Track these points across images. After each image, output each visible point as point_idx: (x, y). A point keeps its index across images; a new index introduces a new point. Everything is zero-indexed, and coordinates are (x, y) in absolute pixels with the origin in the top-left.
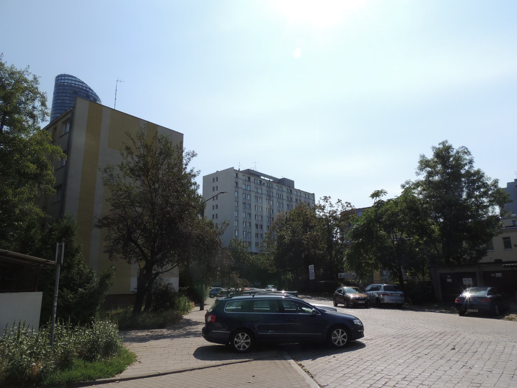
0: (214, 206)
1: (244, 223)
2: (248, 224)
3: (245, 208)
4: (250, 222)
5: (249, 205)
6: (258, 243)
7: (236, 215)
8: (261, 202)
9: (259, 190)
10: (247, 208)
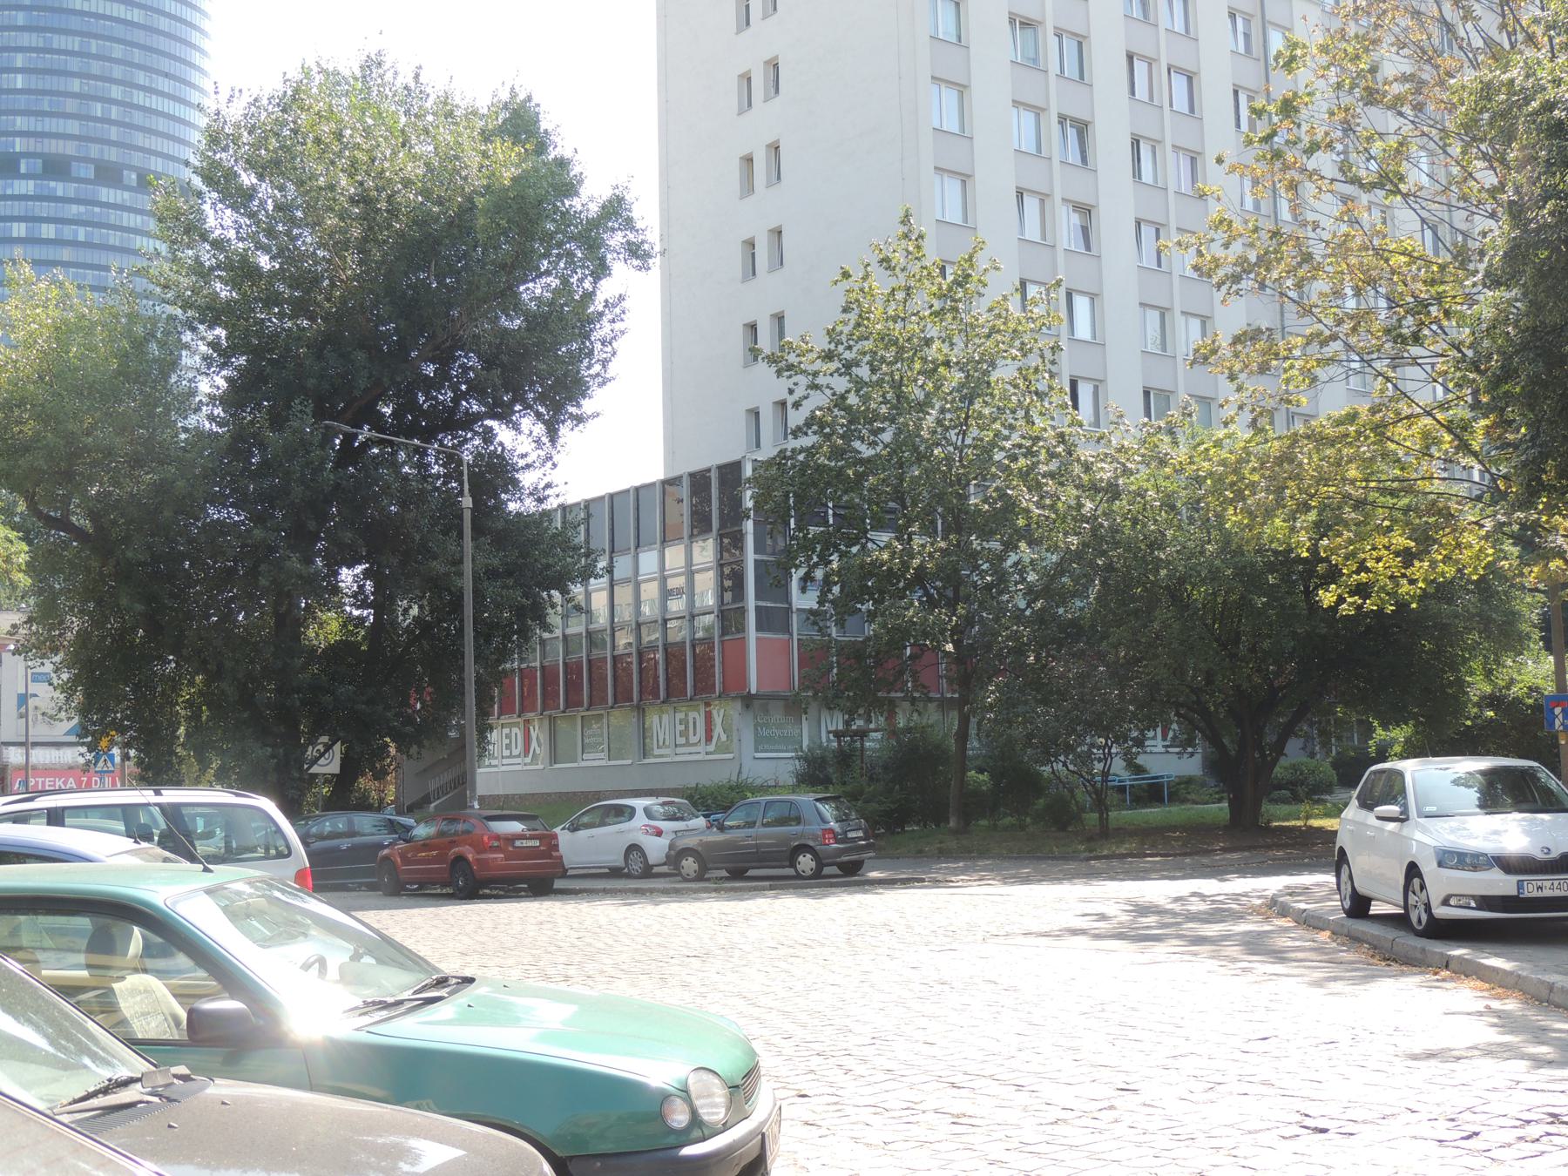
0: (755, 414)
1: (1031, 204)
2: (1067, 224)
3: (1033, 63)
4: (1086, 118)
5: (1070, 46)
6: (1166, 396)
7: (952, 125)
8: (1179, 26)
9: (1180, 320)
10: (1054, 68)
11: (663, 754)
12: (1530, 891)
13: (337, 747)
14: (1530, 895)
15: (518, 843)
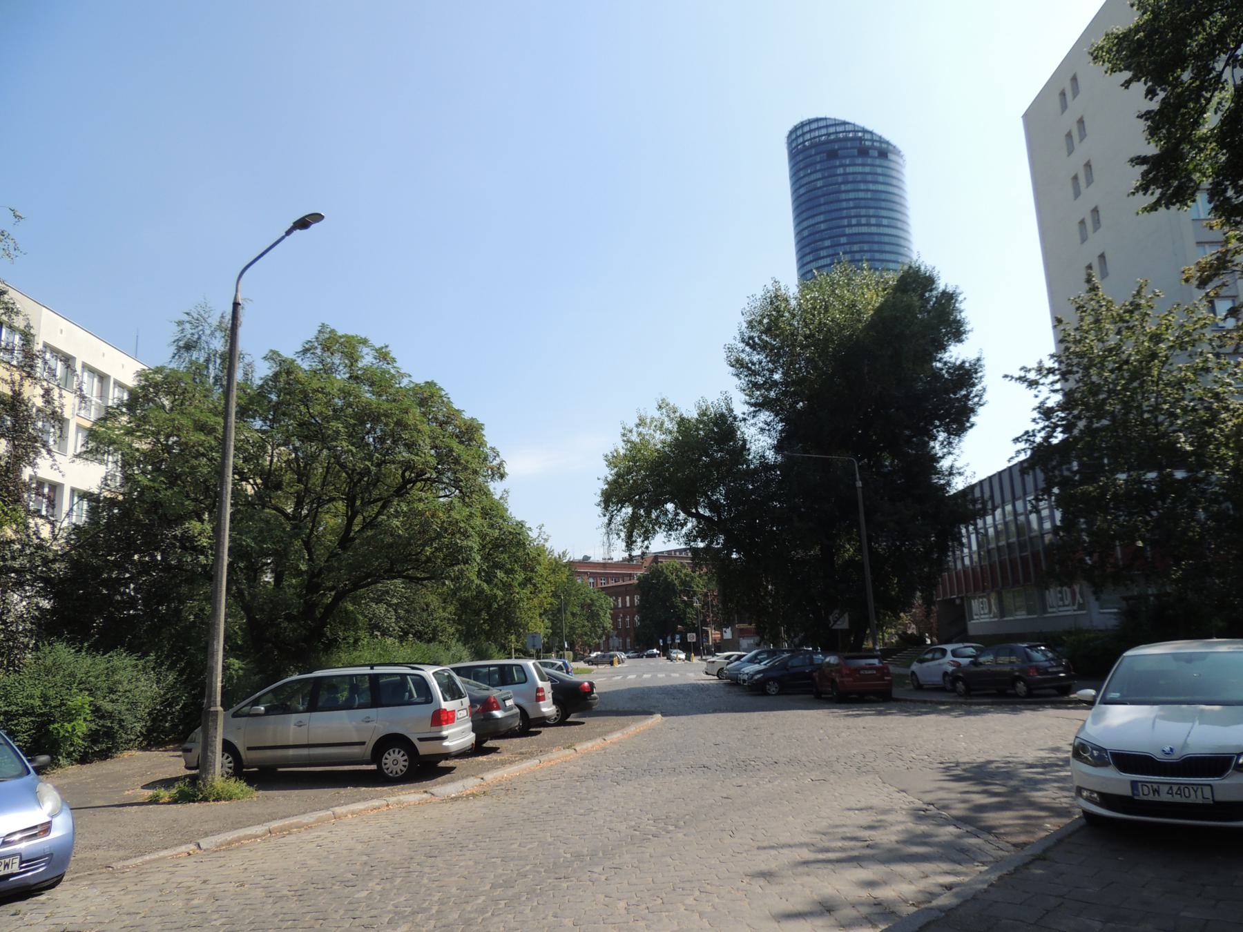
11: (1053, 612)
12: (1145, 795)
13: (846, 615)
14: (1145, 798)
15: (862, 672)
